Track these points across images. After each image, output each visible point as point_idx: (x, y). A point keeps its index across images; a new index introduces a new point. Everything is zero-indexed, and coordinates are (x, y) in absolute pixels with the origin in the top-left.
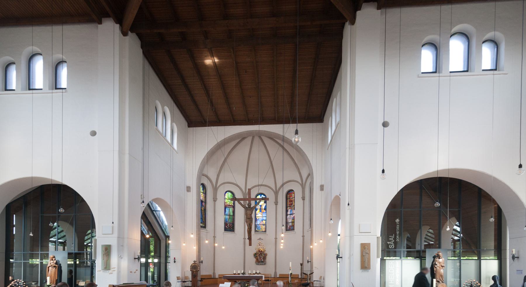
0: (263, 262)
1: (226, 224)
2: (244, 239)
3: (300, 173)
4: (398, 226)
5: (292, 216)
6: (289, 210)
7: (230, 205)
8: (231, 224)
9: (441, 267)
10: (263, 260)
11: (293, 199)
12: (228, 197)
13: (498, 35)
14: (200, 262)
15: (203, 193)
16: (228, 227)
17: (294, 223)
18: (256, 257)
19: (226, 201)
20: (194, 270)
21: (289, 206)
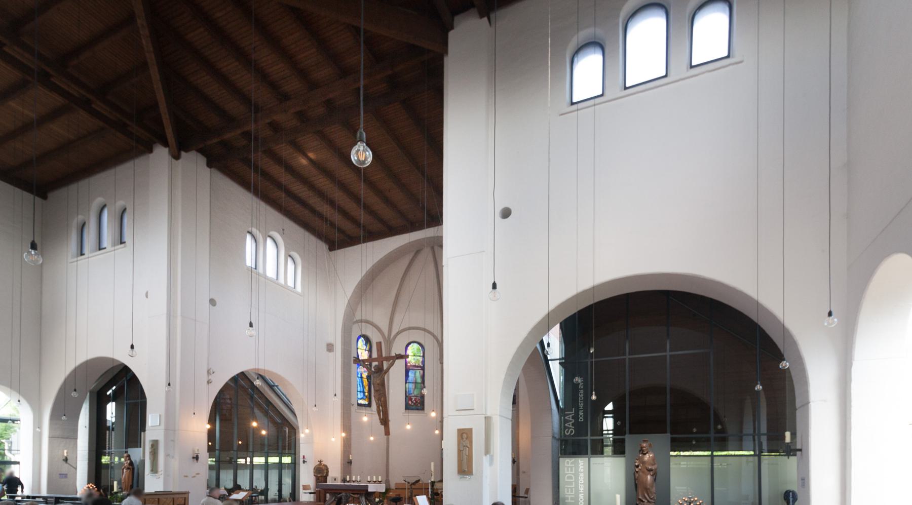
1: (408, 397)
4: (582, 392)
7: (417, 365)
8: (417, 398)
9: (646, 471)
13: (585, 34)
16: (412, 402)
20: (319, 475)
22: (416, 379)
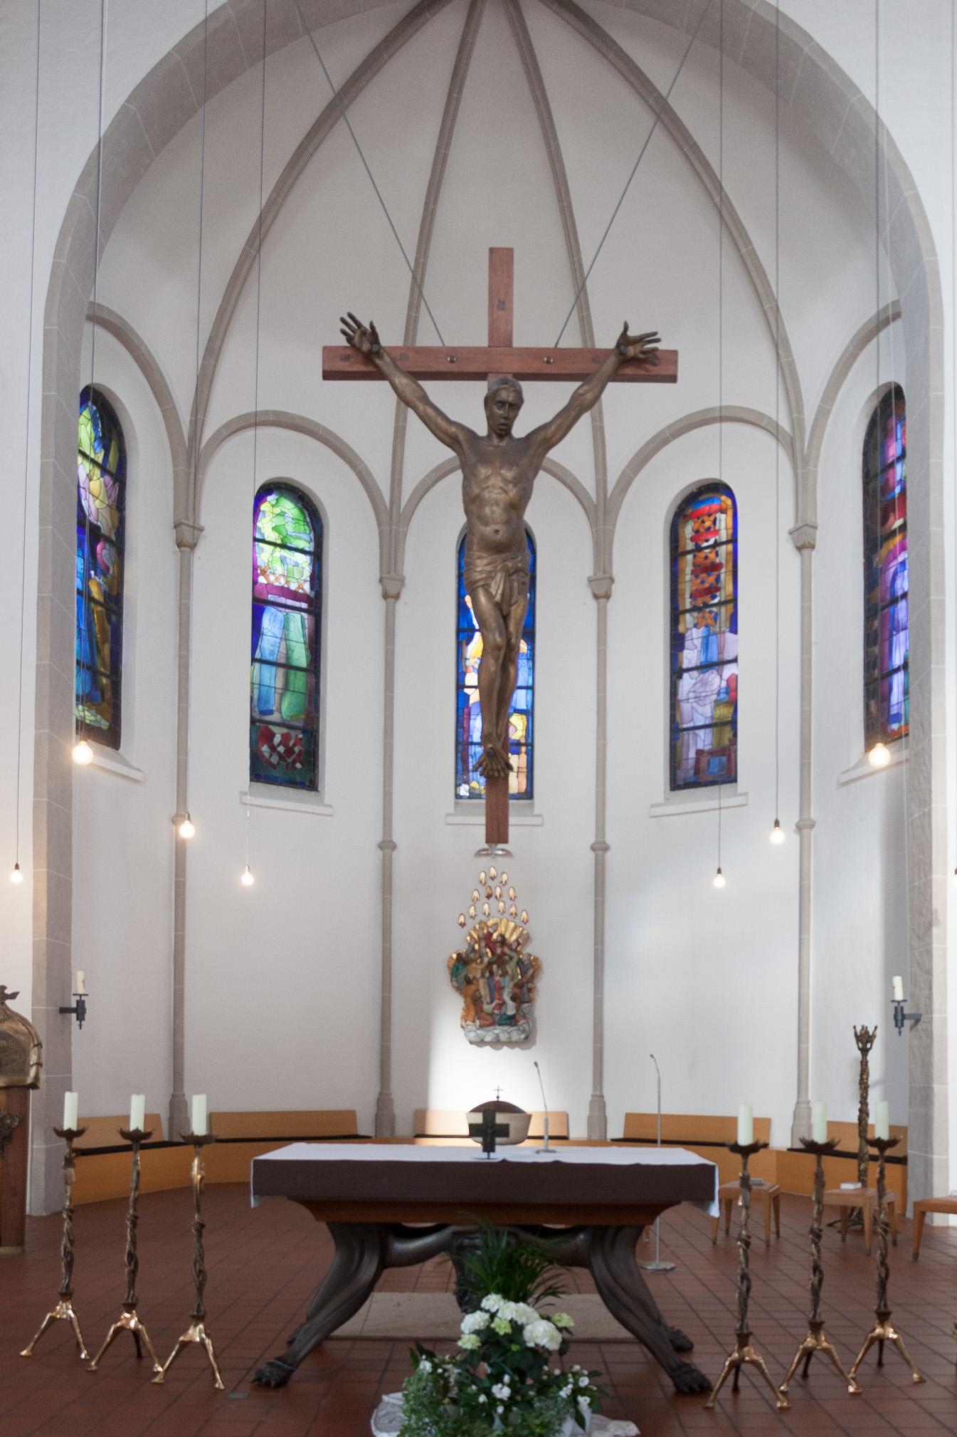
0: (511, 1021)
1: (260, 730)
2: (382, 846)
3: (780, 345)
5: (715, 681)
6: (695, 636)
7: (293, 587)
8: (293, 733)
10: (511, 1009)
11: (723, 550)
12: (275, 529)
14: (64, 1011)
15: (103, 468)
16: (273, 749)
17: (728, 729)
18: (469, 982)
19: (266, 555)
21: (695, 609)
22: (288, 649)
